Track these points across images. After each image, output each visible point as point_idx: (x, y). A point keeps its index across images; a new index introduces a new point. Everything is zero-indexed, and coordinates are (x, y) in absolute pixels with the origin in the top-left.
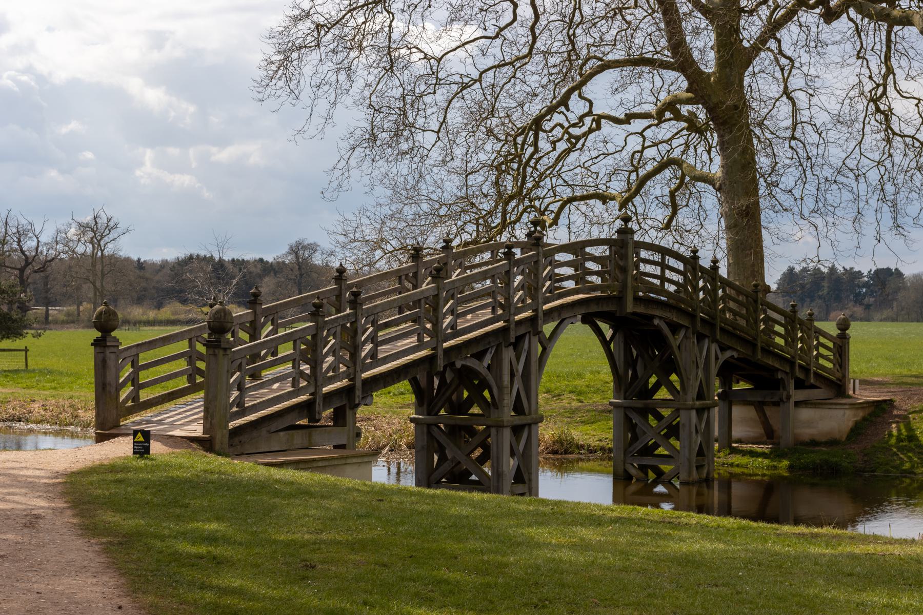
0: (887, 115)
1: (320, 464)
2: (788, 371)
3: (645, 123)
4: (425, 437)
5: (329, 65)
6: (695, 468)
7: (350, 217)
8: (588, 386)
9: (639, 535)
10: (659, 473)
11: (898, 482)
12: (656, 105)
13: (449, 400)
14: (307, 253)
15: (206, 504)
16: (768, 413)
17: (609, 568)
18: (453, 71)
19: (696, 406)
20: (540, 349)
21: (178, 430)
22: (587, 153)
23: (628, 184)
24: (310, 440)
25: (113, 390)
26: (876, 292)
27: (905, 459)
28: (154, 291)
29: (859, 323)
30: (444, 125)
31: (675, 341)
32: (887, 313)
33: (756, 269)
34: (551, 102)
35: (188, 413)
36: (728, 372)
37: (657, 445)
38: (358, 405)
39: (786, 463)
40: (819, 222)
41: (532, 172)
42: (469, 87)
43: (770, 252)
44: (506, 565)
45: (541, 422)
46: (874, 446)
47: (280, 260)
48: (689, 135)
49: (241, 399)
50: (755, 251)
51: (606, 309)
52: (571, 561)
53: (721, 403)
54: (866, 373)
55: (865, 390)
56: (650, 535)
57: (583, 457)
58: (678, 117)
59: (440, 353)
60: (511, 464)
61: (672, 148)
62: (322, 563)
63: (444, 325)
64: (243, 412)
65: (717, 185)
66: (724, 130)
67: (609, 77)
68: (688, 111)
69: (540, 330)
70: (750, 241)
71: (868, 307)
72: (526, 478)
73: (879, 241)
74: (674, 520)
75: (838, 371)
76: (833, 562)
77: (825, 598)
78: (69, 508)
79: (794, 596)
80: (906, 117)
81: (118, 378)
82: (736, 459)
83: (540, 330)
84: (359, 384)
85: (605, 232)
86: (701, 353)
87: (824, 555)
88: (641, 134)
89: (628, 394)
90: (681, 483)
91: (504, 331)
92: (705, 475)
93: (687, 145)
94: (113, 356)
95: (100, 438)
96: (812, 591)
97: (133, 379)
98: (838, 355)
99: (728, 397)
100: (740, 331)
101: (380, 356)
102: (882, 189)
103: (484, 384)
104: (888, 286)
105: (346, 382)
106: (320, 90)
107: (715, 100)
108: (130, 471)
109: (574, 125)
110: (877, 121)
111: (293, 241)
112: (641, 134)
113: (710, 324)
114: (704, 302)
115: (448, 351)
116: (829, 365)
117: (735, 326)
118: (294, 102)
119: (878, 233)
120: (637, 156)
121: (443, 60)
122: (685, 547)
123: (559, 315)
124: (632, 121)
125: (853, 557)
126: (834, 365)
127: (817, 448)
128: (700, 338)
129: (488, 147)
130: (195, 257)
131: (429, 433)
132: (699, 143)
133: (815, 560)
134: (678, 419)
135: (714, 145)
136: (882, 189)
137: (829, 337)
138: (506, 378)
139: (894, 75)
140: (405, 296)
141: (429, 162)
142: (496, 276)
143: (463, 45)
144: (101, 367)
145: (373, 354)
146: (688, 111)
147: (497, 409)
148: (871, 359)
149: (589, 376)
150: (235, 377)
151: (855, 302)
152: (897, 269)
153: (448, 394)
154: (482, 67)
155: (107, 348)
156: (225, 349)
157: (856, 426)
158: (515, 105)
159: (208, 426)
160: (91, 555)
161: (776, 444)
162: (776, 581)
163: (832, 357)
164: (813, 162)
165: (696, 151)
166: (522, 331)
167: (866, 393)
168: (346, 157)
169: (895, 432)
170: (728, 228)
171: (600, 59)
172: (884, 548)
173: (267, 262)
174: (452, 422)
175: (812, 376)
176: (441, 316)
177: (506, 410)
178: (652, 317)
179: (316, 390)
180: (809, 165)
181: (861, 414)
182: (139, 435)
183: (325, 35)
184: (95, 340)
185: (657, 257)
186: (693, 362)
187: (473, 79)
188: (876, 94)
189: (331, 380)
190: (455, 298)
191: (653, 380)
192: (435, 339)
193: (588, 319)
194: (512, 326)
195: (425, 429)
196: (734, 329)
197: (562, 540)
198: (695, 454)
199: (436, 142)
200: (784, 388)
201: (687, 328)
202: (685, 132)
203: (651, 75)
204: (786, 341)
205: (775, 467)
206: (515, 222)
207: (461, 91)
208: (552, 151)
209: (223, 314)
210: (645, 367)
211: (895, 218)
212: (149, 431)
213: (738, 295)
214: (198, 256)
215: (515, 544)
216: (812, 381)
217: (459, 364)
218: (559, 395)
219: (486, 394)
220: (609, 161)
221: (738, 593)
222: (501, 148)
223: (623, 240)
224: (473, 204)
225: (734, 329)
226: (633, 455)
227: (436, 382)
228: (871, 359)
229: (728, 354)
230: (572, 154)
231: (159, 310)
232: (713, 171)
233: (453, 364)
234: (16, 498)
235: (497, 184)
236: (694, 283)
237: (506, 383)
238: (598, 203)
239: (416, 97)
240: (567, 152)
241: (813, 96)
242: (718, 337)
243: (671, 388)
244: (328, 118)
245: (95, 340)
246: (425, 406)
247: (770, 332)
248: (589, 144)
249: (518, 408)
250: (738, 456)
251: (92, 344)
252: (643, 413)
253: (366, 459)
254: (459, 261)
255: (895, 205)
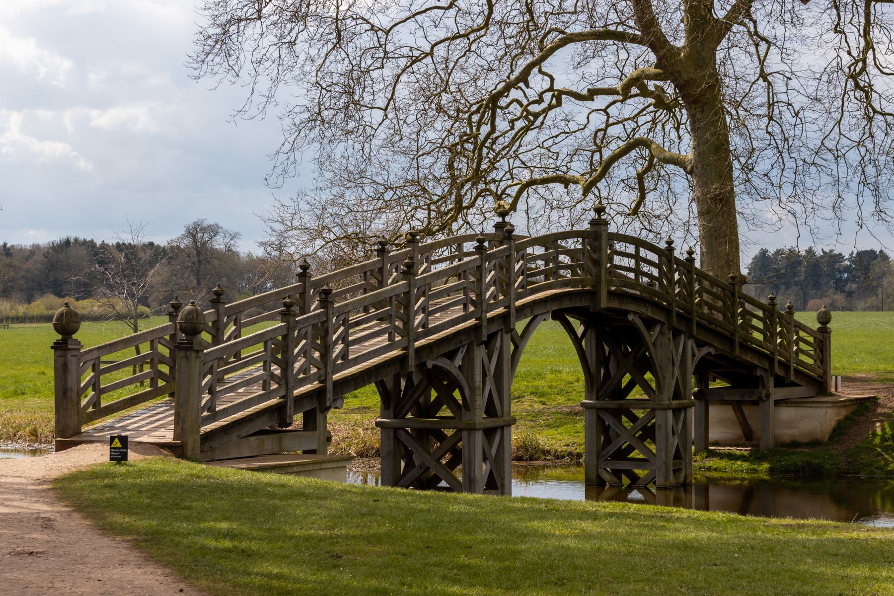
0: (867, 91)
1: (295, 469)
2: (767, 367)
3: (610, 99)
4: (392, 441)
5: (271, 39)
6: (672, 472)
7: (288, 203)
8: (550, 387)
9: (636, 527)
10: (634, 478)
11: (883, 484)
12: (621, 79)
13: (417, 403)
14: (206, 237)
15: (206, 505)
16: (746, 413)
17: (615, 554)
18: (402, 43)
19: (673, 406)
20: (512, 347)
21: (146, 436)
22: (548, 132)
23: (591, 165)
24: (280, 445)
25: (74, 396)
26: (859, 277)
27: (890, 459)
28: (22, 282)
29: (840, 313)
30: (392, 102)
31: (651, 337)
32: (872, 300)
33: (731, 259)
34: (508, 77)
35: (153, 419)
36: (704, 370)
37: (631, 449)
38: (328, 409)
39: (766, 465)
40: (797, 207)
41: (488, 153)
42: (420, 60)
43: (744, 239)
44: (519, 552)
45: (514, 423)
46: (858, 447)
47: (174, 244)
48: (656, 112)
49: (212, 403)
50: (729, 238)
51: (579, 304)
52: (579, 548)
53: (697, 403)
54: (847, 368)
55: (848, 387)
56: (647, 526)
57: (549, 463)
58: (645, 93)
59: (412, 353)
60: (483, 469)
61: (638, 126)
62: (346, 553)
63: (416, 324)
64: (215, 416)
65: (689, 168)
66: (695, 109)
67: (572, 49)
68: (656, 86)
69: (512, 327)
70: (724, 228)
71: (850, 294)
72: (499, 484)
73: (861, 227)
74: (666, 515)
75: (819, 367)
76: (819, 545)
77: (815, 573)
78: (74, 511)
79: (786, 571)
80: (887, 94)
81: (79, 382)
82: (714, 462)
83: (512, 327)
84: (330, 386)
85: (566, 217)
86: (677, 350)
87: (811, 540)
88: (605, 110)
89: (600, 394)
90: (658, 488)
91: (476, 328)
92: (682, 480)
93: (654, 121)
94: (74, 360)
95: (61, 446)
96: (802, 567)
97: (94, 384)
98: (818, 351)
99: (705, 397)
100: (716, 326)
101: (351, 357)
102: (863, 171)
103: (455, 384)
104: (872, 271)
105: (316, 384)
106: (261, 66)
107: (685, 77)
108: (116, 477)
109: (534, 102)
110: (856, 98)
111: (190, 222)
112: (605, 110)
113: (686, 319)
114: (680, 296)
115: (419, 350)
116: (810, 361)
117: (712, 321)
118: (233, 80)
119: (861, 218)
120: (600, 134)
121: (391, 32)
122: (681, 536)
123: (532, 312)
124: (595, 97)
125: (839, 541)
126: (815, 361)
127: (798, 450)
128: (676, 333)
129: (438, 125)
130: (72, 240)
131: (396, 438)
132: (668, 120)
133: (804, 544)
134: (653, 421)
135: (683, 121)
136: (863, 171)
137: (809, 331)
138: (478, 378)
139: (874, 50)
140: (376, 294)
141: (376, 142)
142: (468, 272)
143: (414, 16)
144: (62, 371)
145: (344, 355)
146: (656, 86)
147: (469, 410)
148: (854, 354)
149: (549, 376)
150: (206, 380)
151: (836, 289)
152: (881, 252)
153: (416, 396)
154: (433, 39)
155: (68, 352)
156: (197, 351)
157: (838, 426)
158: (468, 78)
159: (179, 431)
160: (125, 551)
161: (756, 446)
162: (769, 561)
163: (812, 353)
164: (790, 144)
165: (664, 129)
166: (494, 328)
167: (848, 390)
168: (291, 139)
169: (879, 432)
170: (701, 214)
171: (563, 32)
172: (867, 534)
173: (158, 246)
174: (421, 426)
175: (792, 373)
176: (412, 314)
177: (478, 411)
178: (627, 312)
179: (287, 393)
180: (786, 147)
181: (843, 413)
182: (117, 440)
183: (266, 6)
184: (55, 343)
185: (631, 249)
186: (669, 359)
187: (424, 53)
188: (855, 70)
189: (302, 382)
190: (427, 295)
191: (627, 378)
192: (406, 338)
193: (558, 316)
194: (485, 324)
195: (392, 434)
196: (710, 323)
197: (566, 532)
198: (672, 458)
199: (383, 120)
200: (764, 386)
201: (663, 323)
202: (652, 108)
203: (615, 47)
204: (765, 336)
205: (755, 471)
206: (468, 208)
207: (411, 65)
208: (510, 130)
209: (195, 315)
210: (618, 365)
211: (877, 204)
212: (126, 437)
213: (712, 287)
214: (76, 240)
215: (524, 536)
216: (792, 378)
217: (430, 364)
218: (519, 397)
219: (457, 394)
220: (571, 140)
221: (735, 570)
222: (452, 127)
223: (596, 232)
224: (424, 189)
225: (710, 323)
226: (606, 460)
227: (403, 383)
228: (854, 354)
229: (705, 350)
230: (530, 133)
231: (29, 302)
232: (683, 153)
233: (424, 364)
234: (16, 503)
235: (450, 167)
236: (670, 276)
237: (478, 383)
238: (559, 188)
239: (362, 72)
240: (526, 129)
241: (790, 79)
242: (695, 333)
243: (646, 386)
244: (269, 97)
245: (55, 343)
246: (392, 409)
247: (748, 326)
248: (548, 122)
249: (490, 410)
250: (715, 459)
251: (52, 348)
252: (617, 413)
253: (341, 464)
254: (426, 255)
255: (876, 189)
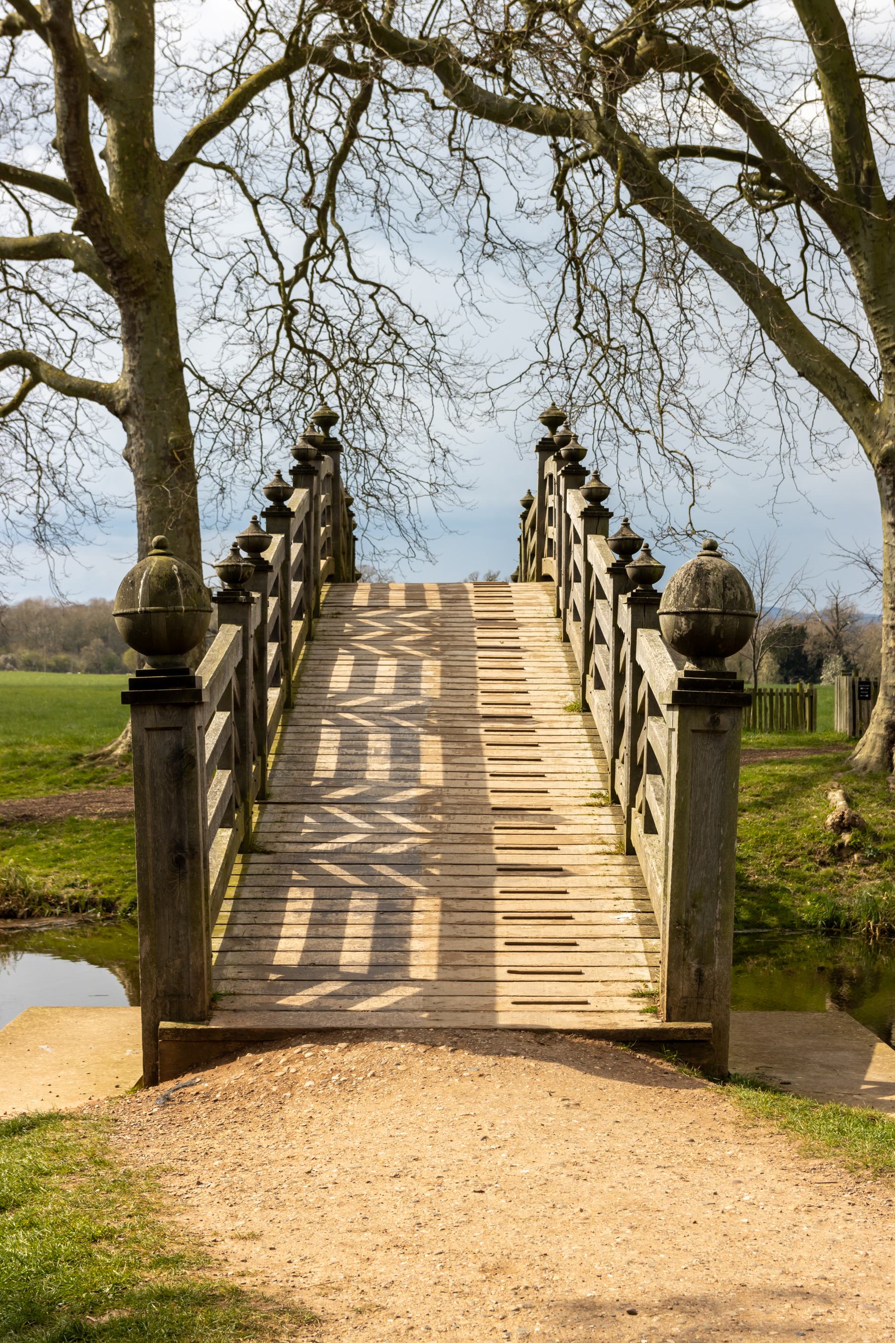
66: (136, 305)
